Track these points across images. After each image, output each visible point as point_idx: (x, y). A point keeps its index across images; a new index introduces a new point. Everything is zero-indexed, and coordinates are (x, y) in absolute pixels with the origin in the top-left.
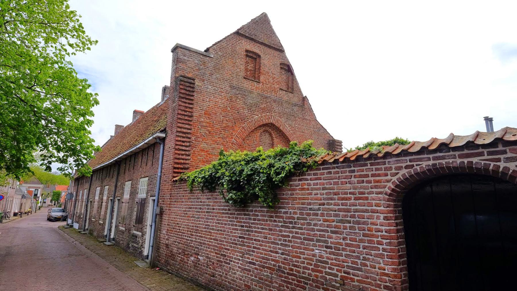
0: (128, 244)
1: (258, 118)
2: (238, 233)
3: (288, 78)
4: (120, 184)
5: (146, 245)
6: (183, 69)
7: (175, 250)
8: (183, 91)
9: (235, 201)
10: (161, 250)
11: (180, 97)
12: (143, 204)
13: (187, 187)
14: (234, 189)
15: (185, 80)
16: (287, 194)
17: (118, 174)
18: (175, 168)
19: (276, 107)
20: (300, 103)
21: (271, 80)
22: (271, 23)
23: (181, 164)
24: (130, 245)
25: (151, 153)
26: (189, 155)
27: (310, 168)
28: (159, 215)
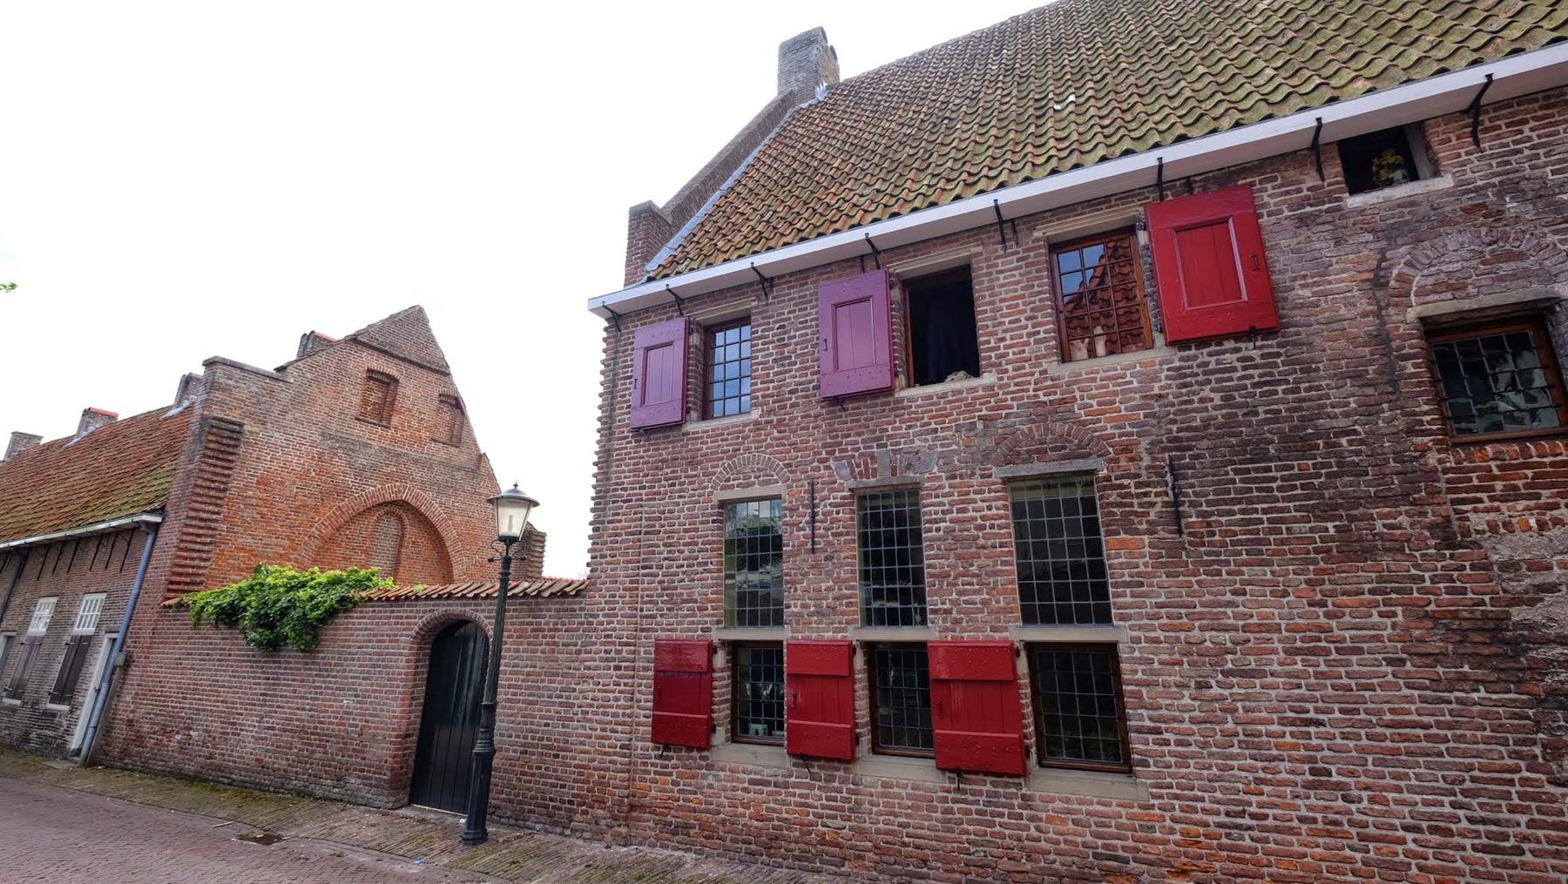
0: (27, 733)
1: (374, 490)
2: (260, 689)
3: (454, 419)
4: (18, 601)
5: (79, 731)
6: (223, 402)
7: (146, 728)
8: (212, 445)
9: (259, 644)
10: (116, 733)
11: (205, 456)
12: (81, 649)
13: (190, 617)
14: (262, 626)
15: (223, 425)
16: (328, 633)
17: (19, 575)
18: (171, 583)
19: (417, 473)
20: (471, 465)
21: (415, 424)
22: (430, 324)
23: (187, 575)
24: (33, 735)
25: (121, 544)
26: (207, 560)
27: (355, 604)
28: (120, 671)
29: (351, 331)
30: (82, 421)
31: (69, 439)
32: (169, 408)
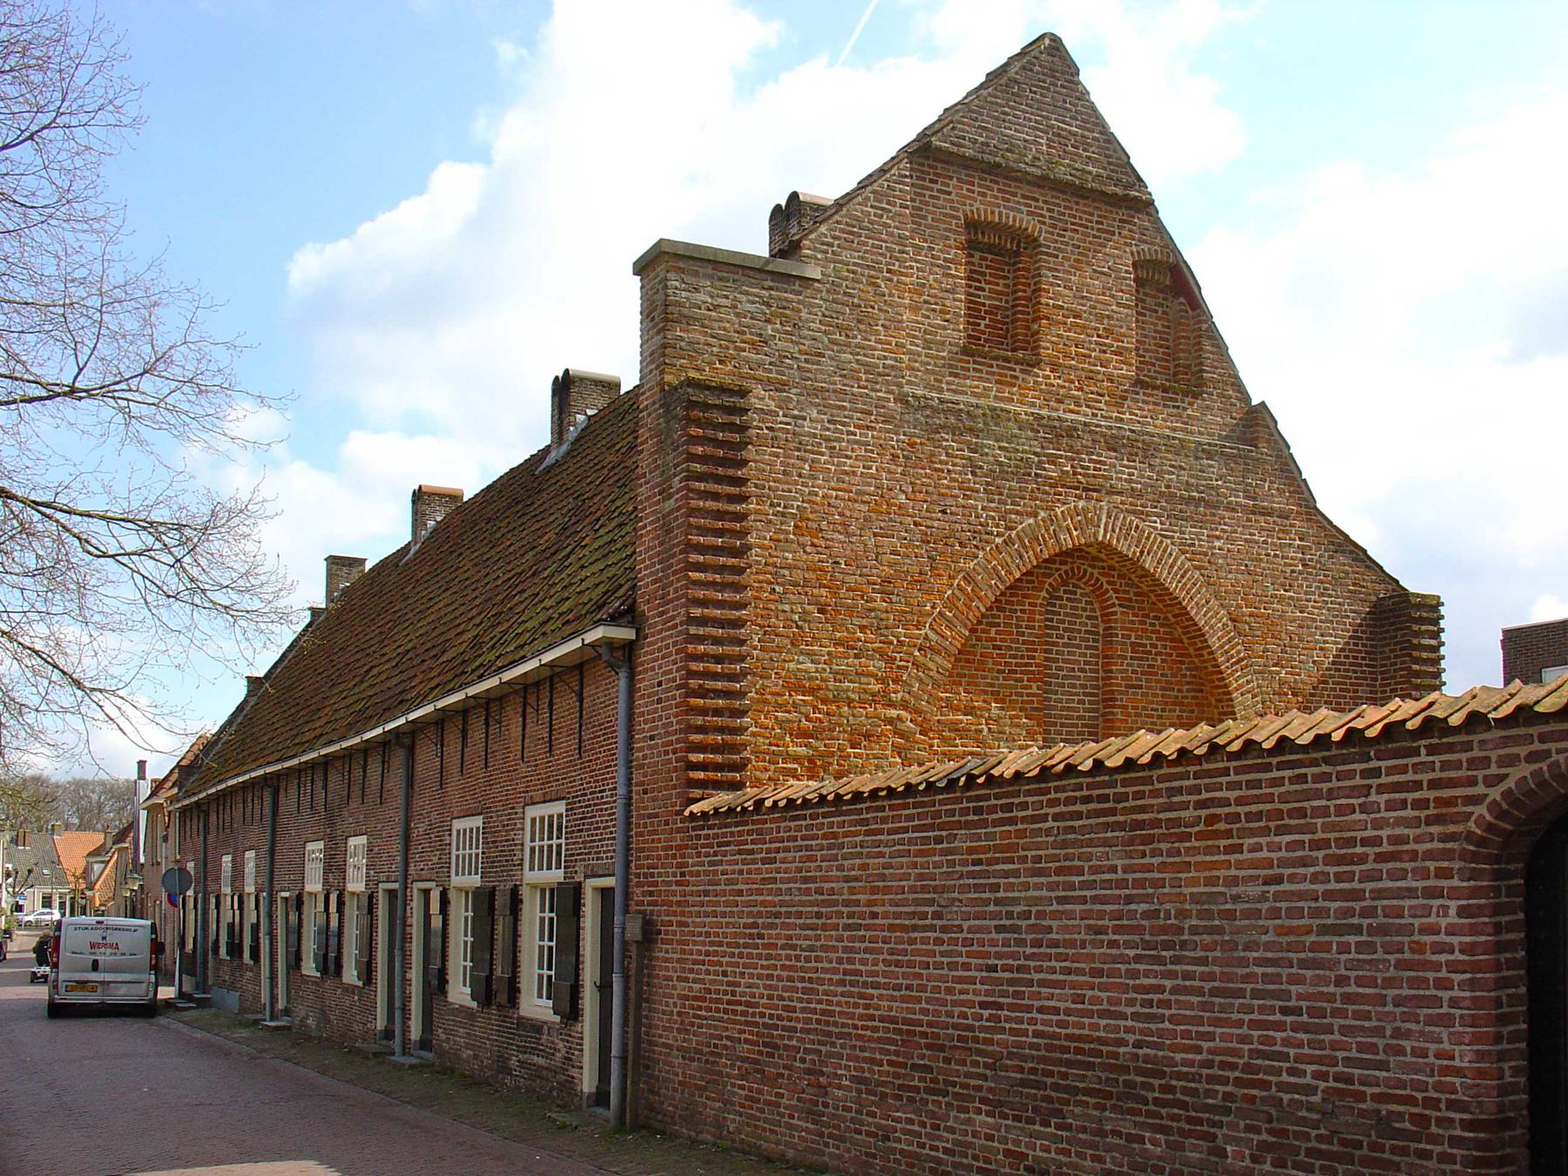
4: (422, 827)
25: (566, 702)
29: (908, 134)
30: (415, 513)
31: (407, 548)
32: (546, 451)
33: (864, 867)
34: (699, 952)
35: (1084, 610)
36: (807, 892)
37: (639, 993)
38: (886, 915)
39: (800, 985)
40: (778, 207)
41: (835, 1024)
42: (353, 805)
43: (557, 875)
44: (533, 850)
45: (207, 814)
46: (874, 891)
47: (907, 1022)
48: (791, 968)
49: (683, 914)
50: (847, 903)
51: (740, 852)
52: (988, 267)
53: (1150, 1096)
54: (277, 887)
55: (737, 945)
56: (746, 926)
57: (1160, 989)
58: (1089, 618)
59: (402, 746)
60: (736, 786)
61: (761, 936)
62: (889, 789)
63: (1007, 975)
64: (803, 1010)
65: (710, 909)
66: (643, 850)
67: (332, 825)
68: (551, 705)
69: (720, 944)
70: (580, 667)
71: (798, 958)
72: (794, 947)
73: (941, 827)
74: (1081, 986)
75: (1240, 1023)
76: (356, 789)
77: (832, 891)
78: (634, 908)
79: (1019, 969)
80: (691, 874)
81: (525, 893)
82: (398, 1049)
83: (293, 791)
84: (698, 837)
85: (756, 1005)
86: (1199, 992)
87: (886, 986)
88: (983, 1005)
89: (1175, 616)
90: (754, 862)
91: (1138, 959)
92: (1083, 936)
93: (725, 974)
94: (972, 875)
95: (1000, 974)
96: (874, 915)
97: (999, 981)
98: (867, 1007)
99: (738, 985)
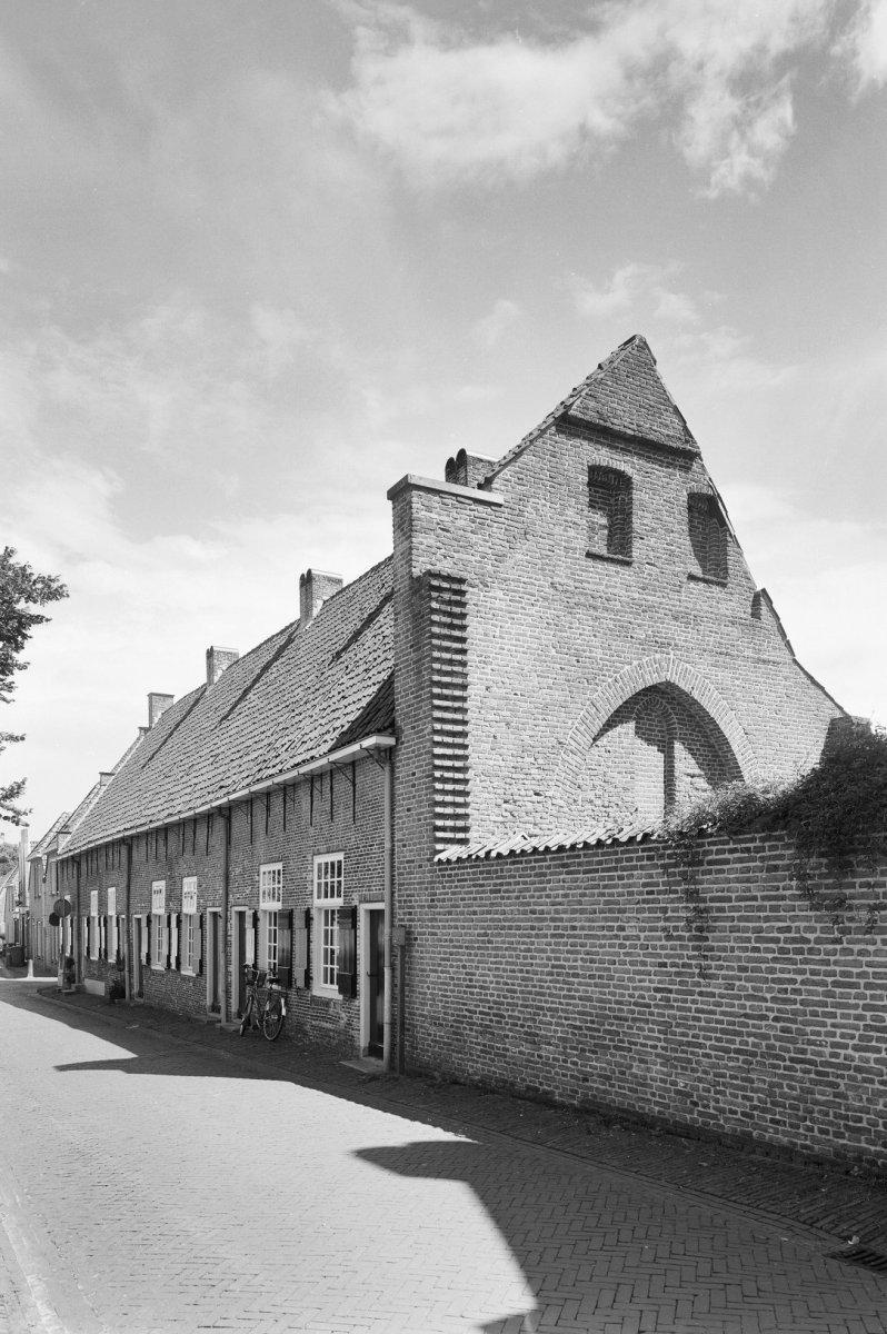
4: (238, 871)
25: (342, 785)
33: (566, 896)
34: (445, 953)
35: (657, 726)
36: (525, 913)
37: (403, 979)
38: (583, 928)
39: (519, 975)
40: (451, 461)
41: (546, 1002)
42: (186, 856)
43: (336, 902)
44: (319, 884)
45: (79, 864)
46: (574, 911)
47: (601, 1001)
48: (513, 964)
49: (433, 927)
50: (553, 920)
51: (474, 886)
52: (600, 497)
53: (787, 1055)
54: (132, 911)
55: (473, 948)
56: (479, 935)
57: (794, 981)
58: (659, 731)
59: (223, 816)
60: (464, 842)
61: (490, 942)
62: (585, 843)
63: (674, 969)
64: (522, 992)
65: (452, 924)
66: (403, 884)
67: (171, 869)
68: (332, 788)
69: (461, 947)
70: (353, 764)
71: (518, 957)
72: (515, 950)
73: (623, 869)
74: (732, 978)
75: (856, 1007)
76: (189, 846)
77: (542, 912)
78: (397, 923)
79: (684, 965)
80: (439, 900)
81: (314, 913)
82: (224, 1019)
83: (143, 848)
84: (443, 876)
85: (488, 988)
86: (824, 984)
87: (584, 977)
88: (657, 990)
89: (711, 730)
90: (483, 892)
91: (775, 960)
92: (732, 944)
93: (464, 967)
94: (644, 901)
95: (669, 969)
96: (574, 928)
97: (669, 974)
98: (569, 990)
99: (474, 974)
